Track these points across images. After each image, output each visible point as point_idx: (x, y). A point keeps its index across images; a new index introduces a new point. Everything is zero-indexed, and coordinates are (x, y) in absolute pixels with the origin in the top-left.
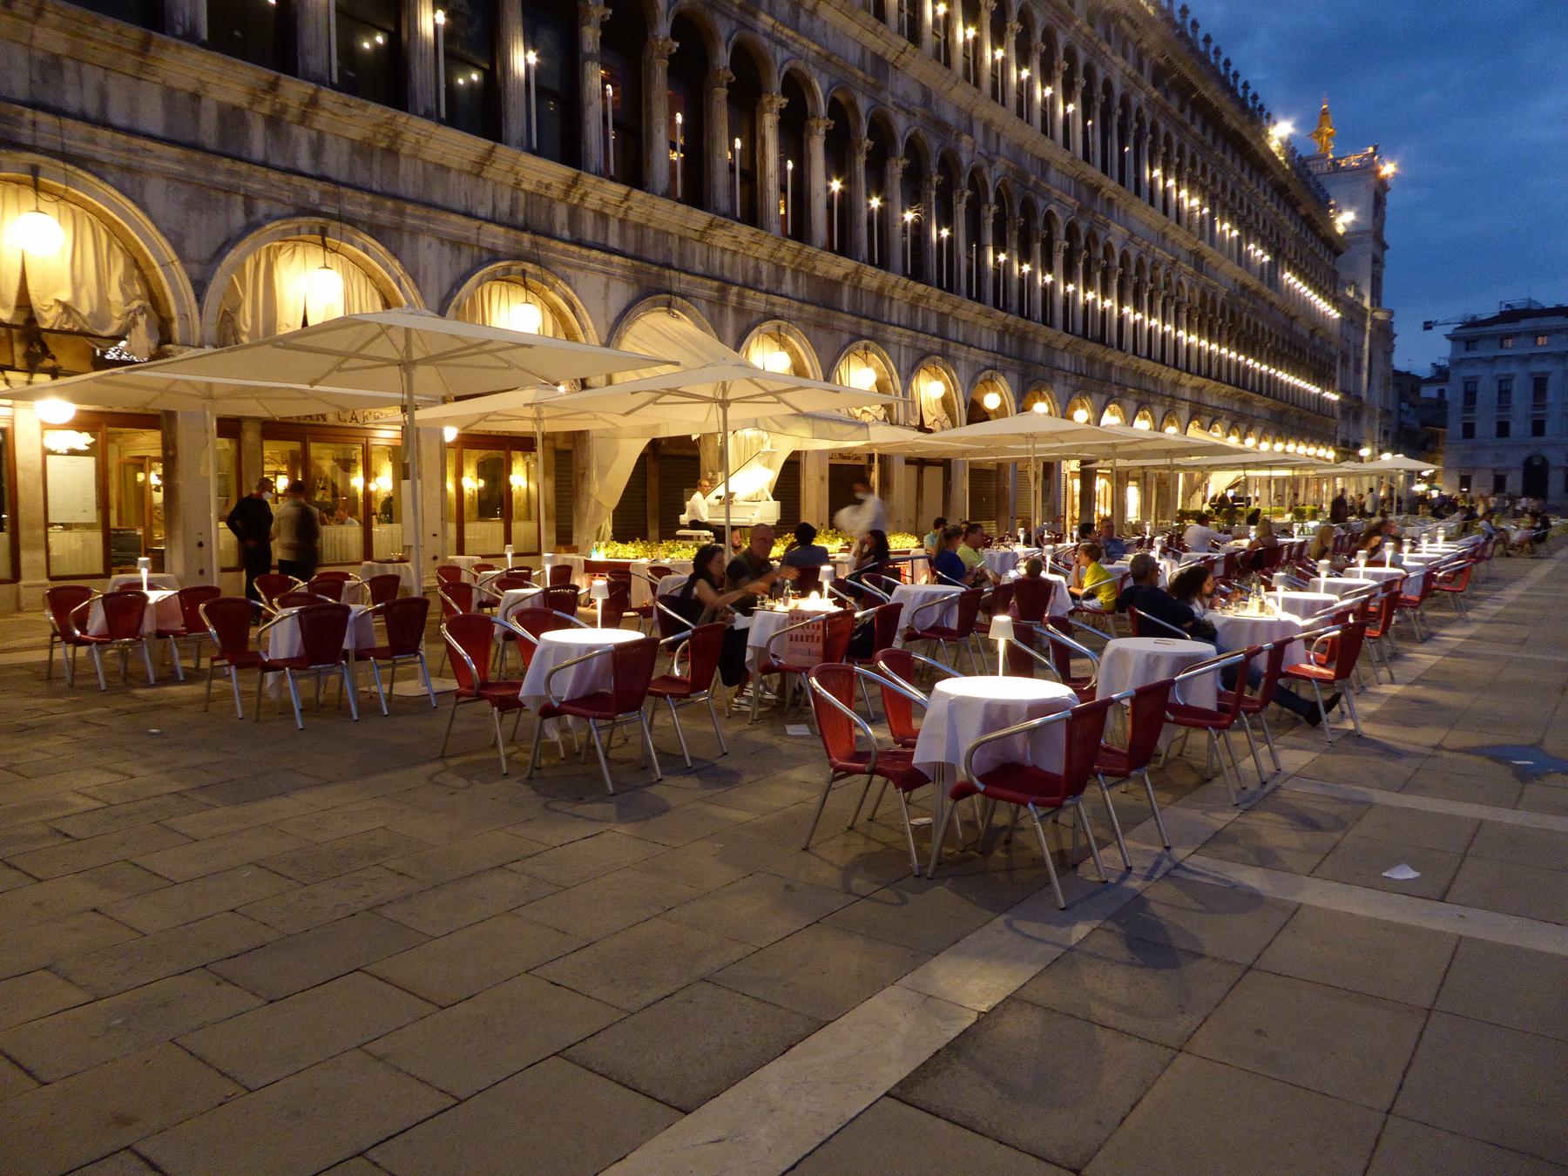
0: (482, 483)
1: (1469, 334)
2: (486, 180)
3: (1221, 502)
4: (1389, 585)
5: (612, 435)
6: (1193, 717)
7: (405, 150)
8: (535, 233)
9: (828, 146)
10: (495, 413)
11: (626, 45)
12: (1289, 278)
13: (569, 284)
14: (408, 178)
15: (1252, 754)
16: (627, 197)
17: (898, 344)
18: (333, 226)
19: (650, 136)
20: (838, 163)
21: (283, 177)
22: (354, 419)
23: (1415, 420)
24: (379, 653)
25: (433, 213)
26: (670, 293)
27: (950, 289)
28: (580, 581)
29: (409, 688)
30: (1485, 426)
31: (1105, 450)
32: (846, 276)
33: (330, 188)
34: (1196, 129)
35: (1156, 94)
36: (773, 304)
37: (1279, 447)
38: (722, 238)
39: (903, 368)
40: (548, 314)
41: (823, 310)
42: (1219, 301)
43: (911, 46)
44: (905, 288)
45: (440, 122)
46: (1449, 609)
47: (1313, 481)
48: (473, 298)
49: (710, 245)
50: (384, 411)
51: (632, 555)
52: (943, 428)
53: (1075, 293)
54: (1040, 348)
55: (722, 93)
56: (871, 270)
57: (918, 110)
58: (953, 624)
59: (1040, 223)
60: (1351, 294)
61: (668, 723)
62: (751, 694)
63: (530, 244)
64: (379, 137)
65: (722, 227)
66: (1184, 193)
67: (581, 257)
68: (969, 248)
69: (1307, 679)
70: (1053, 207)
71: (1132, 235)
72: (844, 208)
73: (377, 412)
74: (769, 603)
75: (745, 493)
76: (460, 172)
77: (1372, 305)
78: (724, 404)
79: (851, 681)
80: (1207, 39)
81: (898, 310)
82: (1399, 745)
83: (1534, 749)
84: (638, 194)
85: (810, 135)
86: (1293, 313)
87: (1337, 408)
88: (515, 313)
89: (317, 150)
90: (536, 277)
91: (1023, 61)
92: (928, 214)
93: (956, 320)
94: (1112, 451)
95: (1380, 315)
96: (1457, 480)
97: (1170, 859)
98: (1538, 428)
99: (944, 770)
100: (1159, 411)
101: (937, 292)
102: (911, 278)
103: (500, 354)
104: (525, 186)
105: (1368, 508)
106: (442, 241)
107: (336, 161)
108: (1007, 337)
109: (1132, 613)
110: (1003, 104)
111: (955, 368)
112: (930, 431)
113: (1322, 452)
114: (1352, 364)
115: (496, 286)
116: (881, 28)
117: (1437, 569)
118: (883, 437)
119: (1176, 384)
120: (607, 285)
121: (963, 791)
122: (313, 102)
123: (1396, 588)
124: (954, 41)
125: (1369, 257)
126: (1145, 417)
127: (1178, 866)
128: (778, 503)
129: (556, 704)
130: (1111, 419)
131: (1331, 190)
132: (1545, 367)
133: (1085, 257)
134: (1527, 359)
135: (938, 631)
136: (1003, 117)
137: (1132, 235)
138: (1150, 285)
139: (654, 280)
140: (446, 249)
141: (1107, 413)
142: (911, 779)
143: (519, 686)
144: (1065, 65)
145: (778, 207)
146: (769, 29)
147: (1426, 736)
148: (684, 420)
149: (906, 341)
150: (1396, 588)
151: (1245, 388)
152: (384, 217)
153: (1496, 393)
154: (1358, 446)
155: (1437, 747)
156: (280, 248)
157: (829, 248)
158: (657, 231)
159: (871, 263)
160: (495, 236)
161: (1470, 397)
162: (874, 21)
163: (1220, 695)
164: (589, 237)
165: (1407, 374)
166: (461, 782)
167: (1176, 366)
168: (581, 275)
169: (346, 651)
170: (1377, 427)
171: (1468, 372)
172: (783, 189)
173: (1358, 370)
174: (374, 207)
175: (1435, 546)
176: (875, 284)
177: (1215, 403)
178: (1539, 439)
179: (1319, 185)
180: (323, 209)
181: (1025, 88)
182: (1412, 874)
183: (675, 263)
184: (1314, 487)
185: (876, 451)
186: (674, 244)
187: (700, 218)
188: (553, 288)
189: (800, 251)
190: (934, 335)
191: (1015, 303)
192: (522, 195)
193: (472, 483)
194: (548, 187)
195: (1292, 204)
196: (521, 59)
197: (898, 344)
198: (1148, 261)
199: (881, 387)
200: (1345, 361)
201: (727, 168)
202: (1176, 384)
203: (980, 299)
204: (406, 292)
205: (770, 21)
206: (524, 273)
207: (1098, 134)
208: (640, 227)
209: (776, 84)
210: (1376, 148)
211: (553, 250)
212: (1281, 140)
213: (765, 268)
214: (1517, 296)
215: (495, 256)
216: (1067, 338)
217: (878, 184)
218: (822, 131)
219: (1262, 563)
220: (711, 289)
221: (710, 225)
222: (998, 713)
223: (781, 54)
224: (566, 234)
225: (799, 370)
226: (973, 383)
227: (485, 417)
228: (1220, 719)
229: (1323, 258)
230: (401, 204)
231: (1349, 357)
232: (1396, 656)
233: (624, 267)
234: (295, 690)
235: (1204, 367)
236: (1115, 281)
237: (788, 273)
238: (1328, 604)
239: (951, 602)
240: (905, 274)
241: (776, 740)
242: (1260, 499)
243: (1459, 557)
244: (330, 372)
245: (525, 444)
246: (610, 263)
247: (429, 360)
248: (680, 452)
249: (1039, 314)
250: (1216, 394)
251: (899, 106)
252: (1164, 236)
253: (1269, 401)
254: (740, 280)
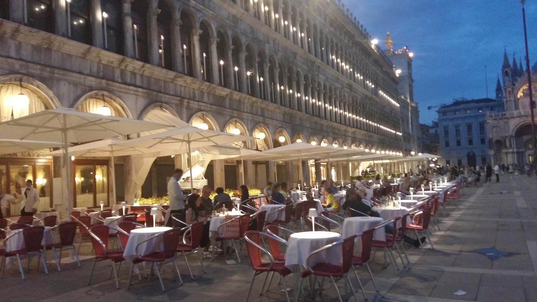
0: (83, 179)
1: (444, 110)
2: (87, 60)
3: (365, 173)
4: (433, 196)
5: (140, 157)
6: (380, 245)
7: (54, 48)
8: (107, 80)
9: (218, 48)
10: (94, 149)
11: (141, 12)
12: (381, 92)
13: (121, 99)
14: (55, 59)
15: (400, 258)
16: (143, 67)
17: (247, 119)
18: (25, 78)
19: (151, 44)
20: (222, 55)
21: (4, 59)
22: (29, 155)
23: (428, 141)
24: (57, 246)
25: (66, 72)
26: (161, 102)
27: (265, 99)
29: (66, 260)
30: (453, 143)
31: (325, 155)
32: (227, 95)
33: (24, 63)
35: (332, 29)
36: (201, 106)
37: (383, 152)
38: (180, 81)
39: (249, 128)
40: (113, 111)
41: (219, 108)
42: (358, 101)
43: (246, 13)
44: (249, 99)
45: (69, 38)
46: (452, 205)
47: (396, 164)
48: (82, 105)
49: (176, 85)
50: (42, 151)
51: (150, 203)
52: (265, 150)
53: (309, 100)
54: (298, 119)
55: (178, 28)
56: (236, 93)
57: (250, 35)
58: (283, 218)
59: (295, 75)
60: (403, 98)
61: (180, 263)
62: (211, 250)
63: (106, 85)
64: (44, 43)
65: (180, 77)
66: (343, 64)
67: (126, 89)
68: (270, 84)
69: (413, 229)
70: (299, 69)
71: (327, 78)
72: (225, 71)
73: (39, 152)
74: (217, 214)
75: (195, 177)
76: (77, 57)
77: (410, 101)
78: (189, 142)
79: (258, 237)
80: (348, 10)
81: (246, 107)
82: (447, 251)
83: (493, 249)
84: (148, 65)
85: (211, 44)
86: (384, 105)
87: (402, 138)
88: (100, 109)
89: (19, 48)
90: (108, 97)
91: (285, 19)
92: (255, 72)
93: (268, 110)
94: (328, 155)
95: (413, 105)
96: (445, 162)
97: (379, 295)
98: (471, 142)
99: (296, 267)
100: (341, 141)
101: (260, 100)
102: (251, 95)
103: (103, 125)
104: (103, 62)
106: (69, 84)
107: (26, 53)
108: (286, 116)
109: (349, 210)
110: (279, 33)
111: (268, 128)
112: (261, 151)
113: (398, 154)
114: (406, 123)
115: (92, 101)
116: (235, 6)
117: (447, 191)
118: (245, 153)
119: (346, 131)
120: (136, 99)
121: (306, 274)
122: (17, 31)
123: (436, 197)
124: (261, 10)
125: (408, 85)
126: (336, 144)
127: (383, 297)
128: (206, 180)
129: (140, 258)
130: (324, 144)
131: (393, 61)
132: (470, 121)
133: (311, 88)
134: (464, 118)
135: (278, 222)
136: (279, 37)
137: (327, 78)
138: (335, 96)
139: (155, 97)
140: (72, 86)
141: (323, 143)
142: (285, 272)
143: (123, 252)
144: (300, 19)
145: (200, 70)
146: (194, 6)
147: (456, 248)
148: (168, 150)
149: (250, 118)
150: (436, 197)
151: (370, 132)
152: (46, 74)
153: (455, 131)
154: (410, 151)
155: (461, 251)
156: (2, 87)
157: (220, 85)
158: (155, 79)
159: (236, 90)
160: (91, 81)
161: (446, 132)
162: (232, 3)
163: (386, 236)
164: (129, 81)
165: (424, 125)
166: (100, 293)
167: (346, 125)
168: (126, 96)
169: (42, 246)
170: (416, 144)
171: (444, 123)
172: (202, 63)
173: (408, 124)
174: (42, 70)
175: (444, 184)
176: (238, 97)
177: (360, 137)
178: (471, 146)
179: (389, 60)
180: (20, 71)
181: (287, 28)
182: (463, 293)
183: (162, 90)
184: (396, 166)
185: (242, 159)
186: (162, 84)
187: (171, 74)
188: (115, 101)
189: (210, 86)
190: (260, 116)
191: (288, 103)
192: (101, 65)
193: (79, 179)
194: (112, 62)
195: (381, 67)
196: (101, 15)
197: (247, 119)
198: (333, 88)
199: (242, 134)
201: (181, 56)
202: (346, 131)
203: (275, 102)
204: (55, 105)
205: (194, 2)
206: (103, 95)
207: (313, 43)
208: (149, 78)
209: (198, 25)
210: (407, 47)
211: (114, 86)
212: (375, 45)
213: (197, 92)
214: (458, 96)
215: (91, 89)
216: (307, 115)
217: (237, 62)
218: (215, 42)
219: (387, 192)
220: (177, 100)
221: (176, 77)
222: (315, 244)
223: (199, 15)
224: (120, 80)
225: (211, 128)
226: (275, 133)
227: (89, 151)
228: (388, 244)
229: (392, 86)
230: (53, 69)
231: (404, 119)
232: (439, 222)
233: (143, 92)
234: (20, 263)
235: (355, 124)
236: (322, 95)
237: (206, 94)
238: (415, 203)
239: (282, 210)
240: (248, 94)
241: (223, 266)
242: (381, 171)
243: (454, 186)
244: (30, 134)
245: (104, 162)
246: (138, 91)
247: (73, 128)
248: (164, 163)
249: (297, 107)
250: (360, 134)
251: (242, 33)
252: (338, 79)
253: (379, 136)
254: (188, 97)
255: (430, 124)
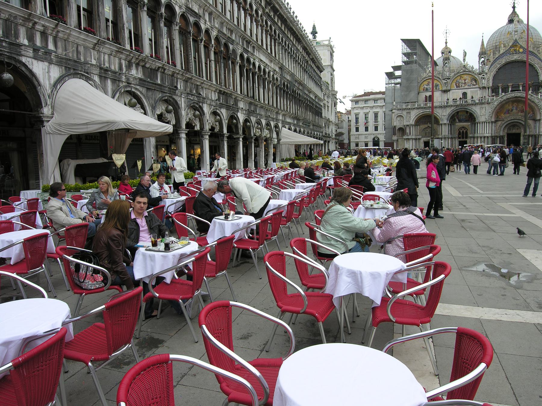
1: (356, 100)
28: (100, 216)
34: (279, 24)
93: (202, 88)
98: (376, 129)
161: (357, 119)
200: (324, 107)
255: (344, 111)
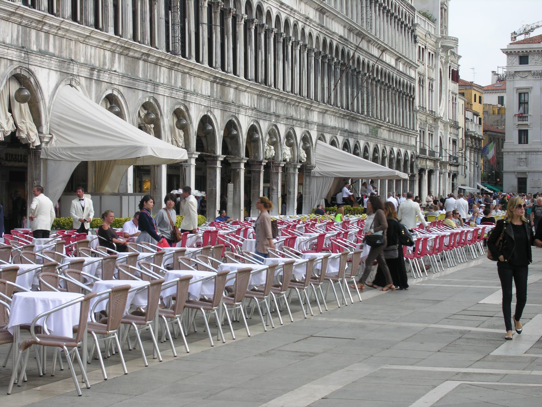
105: (51, 136)
171: (521, 84)
